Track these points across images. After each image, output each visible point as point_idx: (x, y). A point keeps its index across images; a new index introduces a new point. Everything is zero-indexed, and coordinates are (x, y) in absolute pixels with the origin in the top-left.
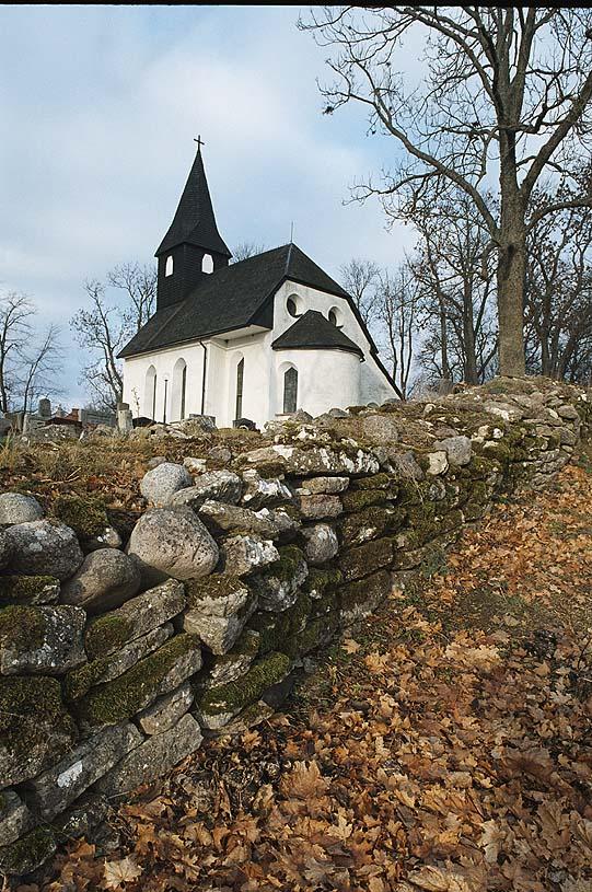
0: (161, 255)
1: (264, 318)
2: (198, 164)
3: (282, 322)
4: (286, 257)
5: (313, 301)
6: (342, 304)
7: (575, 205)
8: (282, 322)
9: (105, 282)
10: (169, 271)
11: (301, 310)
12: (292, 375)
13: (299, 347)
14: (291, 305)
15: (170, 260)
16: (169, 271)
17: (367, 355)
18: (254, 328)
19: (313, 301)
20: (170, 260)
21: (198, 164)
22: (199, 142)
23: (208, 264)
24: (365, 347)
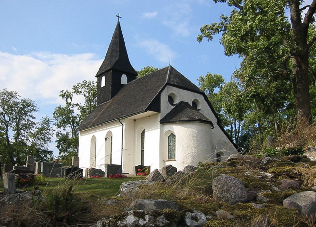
0: (99, 76)
1: (155, 106)
2: (119, 29)
3: (166, 108)
4: (167, 73)
5: (183, 96)
6: (200, 98)
7: (297, 66)
8: (166, 108)
9: (72, 90)
10: (103, 84)
11: (177, 102)
12: (172, 136)
13: (103, 64)
14: (171, 99)
15: (103, 79)
16: (103, 84)
17: (216, 125)
18: (149, 112)
19: (183, 96)
20: (103, 79)
21: (119, 29)
22: (119, 17)
23: (124, 79)
24: (214, 120)
